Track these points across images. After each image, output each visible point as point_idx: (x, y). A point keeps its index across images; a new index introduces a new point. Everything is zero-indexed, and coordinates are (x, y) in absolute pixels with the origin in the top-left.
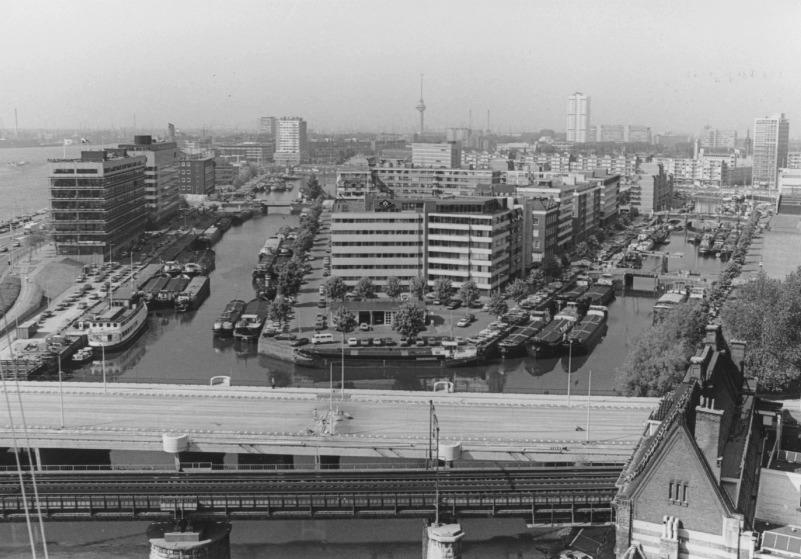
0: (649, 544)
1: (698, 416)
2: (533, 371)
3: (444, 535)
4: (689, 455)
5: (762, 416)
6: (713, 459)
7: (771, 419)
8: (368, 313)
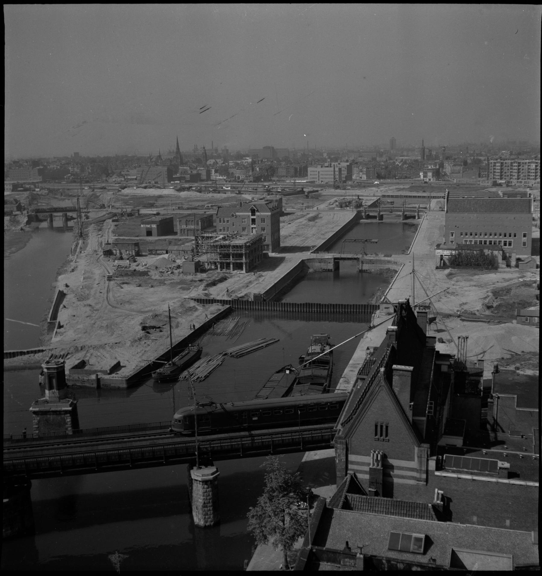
0: (361, 472)
1: (394, 373)
2: (240, 299)
3: (203, 475)
4: (389, 403)
5: (441, 365)
6: (405, 398)
7: (447, 367)
8: (400, 534)
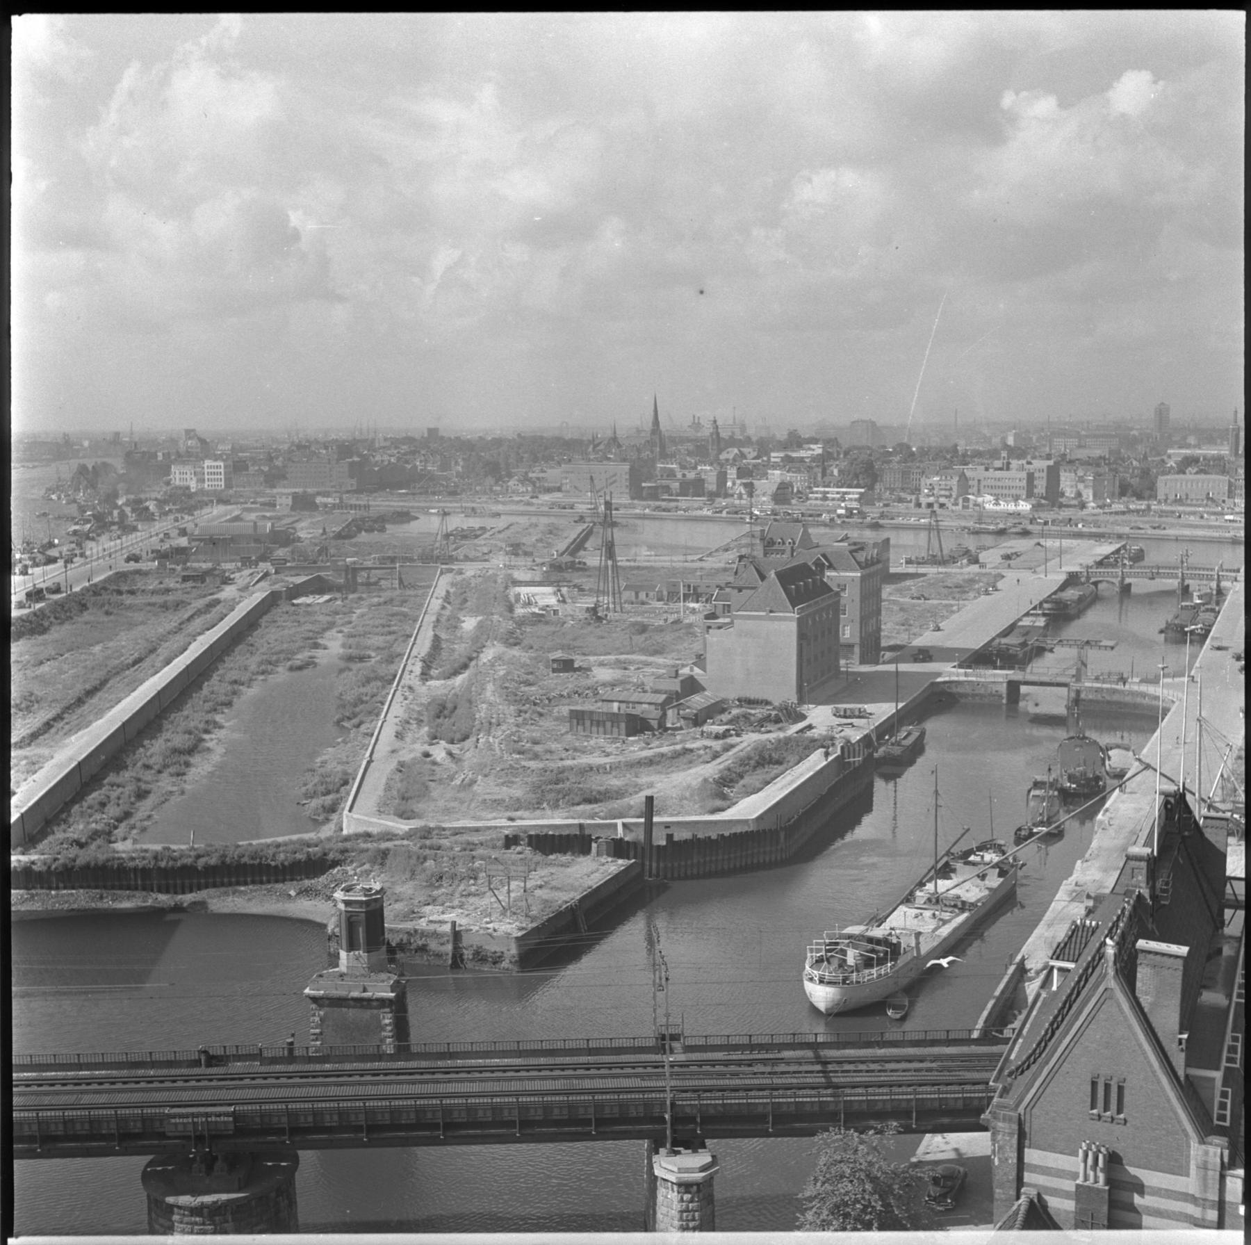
0: (1056, 1192)
